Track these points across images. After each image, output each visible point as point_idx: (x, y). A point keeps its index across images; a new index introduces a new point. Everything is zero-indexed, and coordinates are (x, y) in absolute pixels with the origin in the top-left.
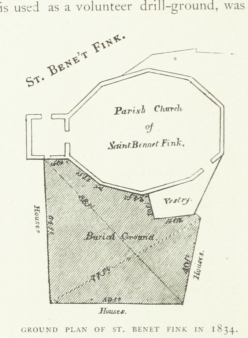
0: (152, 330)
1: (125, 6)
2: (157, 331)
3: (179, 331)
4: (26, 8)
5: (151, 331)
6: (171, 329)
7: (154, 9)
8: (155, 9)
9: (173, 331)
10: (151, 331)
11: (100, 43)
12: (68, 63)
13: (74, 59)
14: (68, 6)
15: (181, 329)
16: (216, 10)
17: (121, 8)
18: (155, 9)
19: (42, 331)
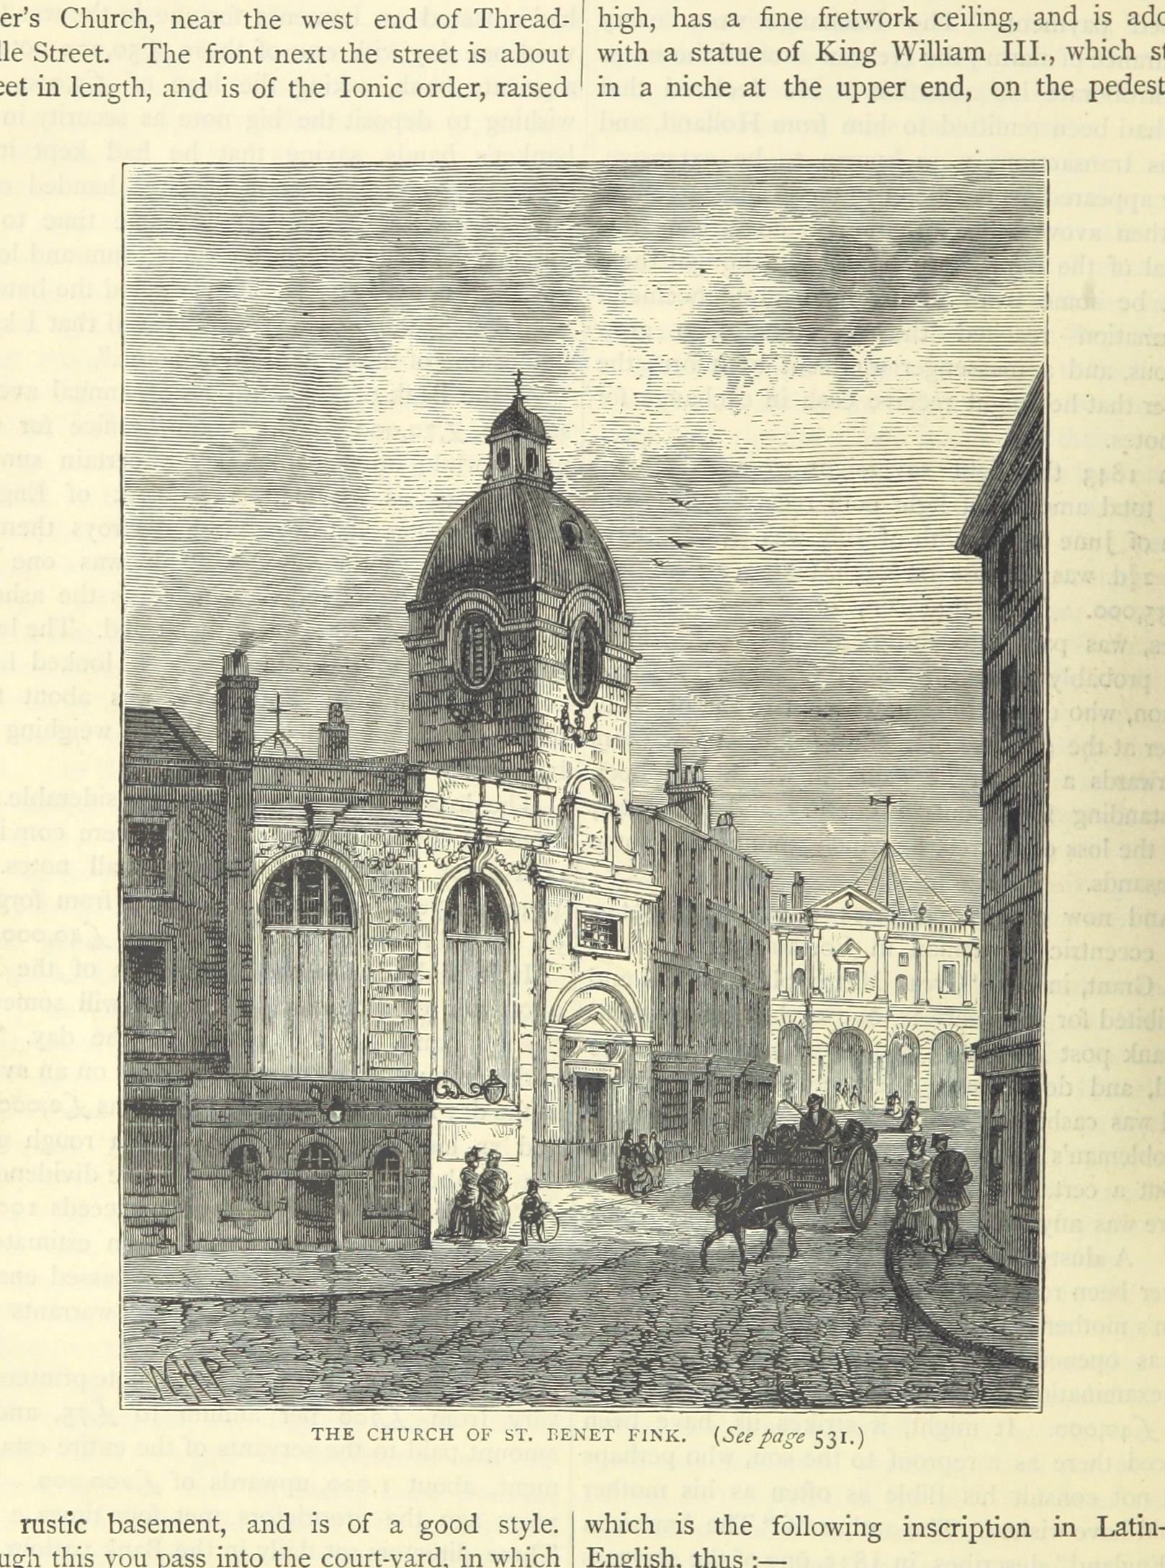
0: (348, 1437)
1: (550, 87)
2: (608, 1439)
3: (584, 1438)
4: (538, 88)
5: (592, 1439)
6: (641, 1435)
7: (1037, 44)
8: (1034, 42)
9: (644, 1440)
10: (592, 1439)
11: (781, 1444)
12: (1065, 1529)
13: (346, 1430)
14: (673, 50)
15: (664, 1435)
16: (967, 97)
17: (334, 1562)
18: (1034, 42)
19: (403, 1437)
